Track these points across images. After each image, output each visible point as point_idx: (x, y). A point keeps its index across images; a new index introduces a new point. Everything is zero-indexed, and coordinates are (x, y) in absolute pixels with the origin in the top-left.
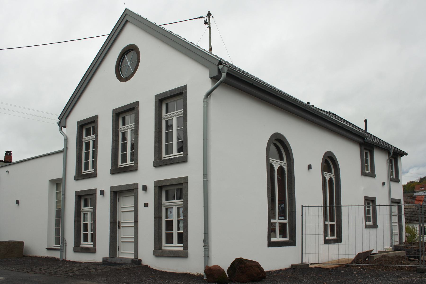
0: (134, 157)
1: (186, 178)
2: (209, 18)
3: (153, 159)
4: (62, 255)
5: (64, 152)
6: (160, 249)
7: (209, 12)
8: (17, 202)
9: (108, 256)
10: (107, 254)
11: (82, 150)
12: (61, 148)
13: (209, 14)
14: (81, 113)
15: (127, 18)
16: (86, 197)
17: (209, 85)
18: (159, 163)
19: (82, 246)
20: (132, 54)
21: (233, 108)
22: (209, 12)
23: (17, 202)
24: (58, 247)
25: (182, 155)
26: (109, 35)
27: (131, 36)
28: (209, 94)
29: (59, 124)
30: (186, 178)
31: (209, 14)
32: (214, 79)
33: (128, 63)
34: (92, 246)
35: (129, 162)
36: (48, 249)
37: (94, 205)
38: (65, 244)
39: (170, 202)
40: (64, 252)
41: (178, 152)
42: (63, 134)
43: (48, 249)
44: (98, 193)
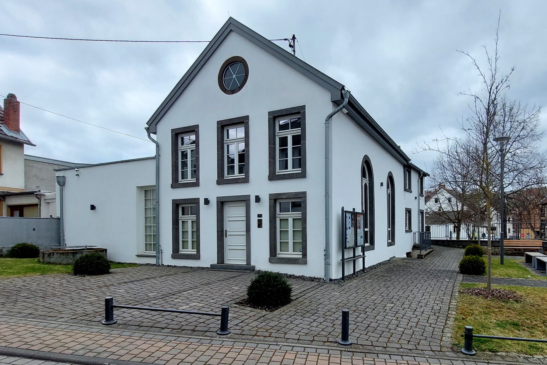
0: (196, 173)
1: (305, 193)
2: (294, 41)
3: (216, 178)
4: (157, 261)
5: (157, 158)
6: (275, 256)
7: (294, 35)
8: (93, 208)
9: (215, 262)
10: (214, 260)
11: (178, 159)
12: (153, 154)
13: (294, 38)
14: (177, 119)
15: (231, 27)
16: (184, 206)
17: (330, 108)
18: (221, 181)
19: (180, 252)
20: (239, 66)
21: (345, 132)
22: (294, 35)
23: (93, 208)
24: (153, 253)
25: (300, 172)
26: (210, 42)
27: (234, 47)
28: (330, 116)
29: (148, 129)
30: (305, 193)
31: (294, 38)
32: (336, 103)
33: (234, 74)
34: (196, 253)
35: (290, 169)
36: (138, 256)
37: (197, 212)
38: (160, 251)
39: (284, 215)
40: (160, 259)
41: (293, 168)
42: (153, 141)
43: (138, 256)
44: (202, 202)
